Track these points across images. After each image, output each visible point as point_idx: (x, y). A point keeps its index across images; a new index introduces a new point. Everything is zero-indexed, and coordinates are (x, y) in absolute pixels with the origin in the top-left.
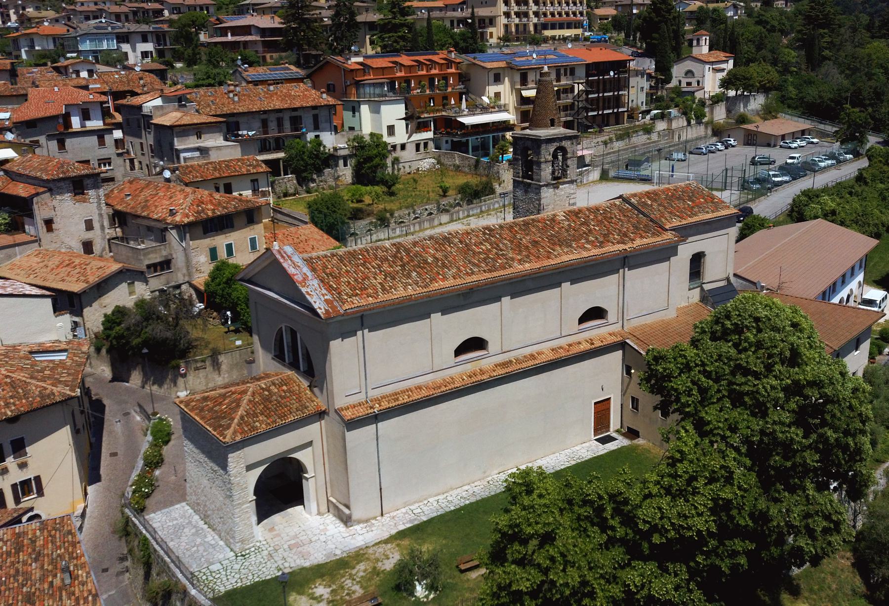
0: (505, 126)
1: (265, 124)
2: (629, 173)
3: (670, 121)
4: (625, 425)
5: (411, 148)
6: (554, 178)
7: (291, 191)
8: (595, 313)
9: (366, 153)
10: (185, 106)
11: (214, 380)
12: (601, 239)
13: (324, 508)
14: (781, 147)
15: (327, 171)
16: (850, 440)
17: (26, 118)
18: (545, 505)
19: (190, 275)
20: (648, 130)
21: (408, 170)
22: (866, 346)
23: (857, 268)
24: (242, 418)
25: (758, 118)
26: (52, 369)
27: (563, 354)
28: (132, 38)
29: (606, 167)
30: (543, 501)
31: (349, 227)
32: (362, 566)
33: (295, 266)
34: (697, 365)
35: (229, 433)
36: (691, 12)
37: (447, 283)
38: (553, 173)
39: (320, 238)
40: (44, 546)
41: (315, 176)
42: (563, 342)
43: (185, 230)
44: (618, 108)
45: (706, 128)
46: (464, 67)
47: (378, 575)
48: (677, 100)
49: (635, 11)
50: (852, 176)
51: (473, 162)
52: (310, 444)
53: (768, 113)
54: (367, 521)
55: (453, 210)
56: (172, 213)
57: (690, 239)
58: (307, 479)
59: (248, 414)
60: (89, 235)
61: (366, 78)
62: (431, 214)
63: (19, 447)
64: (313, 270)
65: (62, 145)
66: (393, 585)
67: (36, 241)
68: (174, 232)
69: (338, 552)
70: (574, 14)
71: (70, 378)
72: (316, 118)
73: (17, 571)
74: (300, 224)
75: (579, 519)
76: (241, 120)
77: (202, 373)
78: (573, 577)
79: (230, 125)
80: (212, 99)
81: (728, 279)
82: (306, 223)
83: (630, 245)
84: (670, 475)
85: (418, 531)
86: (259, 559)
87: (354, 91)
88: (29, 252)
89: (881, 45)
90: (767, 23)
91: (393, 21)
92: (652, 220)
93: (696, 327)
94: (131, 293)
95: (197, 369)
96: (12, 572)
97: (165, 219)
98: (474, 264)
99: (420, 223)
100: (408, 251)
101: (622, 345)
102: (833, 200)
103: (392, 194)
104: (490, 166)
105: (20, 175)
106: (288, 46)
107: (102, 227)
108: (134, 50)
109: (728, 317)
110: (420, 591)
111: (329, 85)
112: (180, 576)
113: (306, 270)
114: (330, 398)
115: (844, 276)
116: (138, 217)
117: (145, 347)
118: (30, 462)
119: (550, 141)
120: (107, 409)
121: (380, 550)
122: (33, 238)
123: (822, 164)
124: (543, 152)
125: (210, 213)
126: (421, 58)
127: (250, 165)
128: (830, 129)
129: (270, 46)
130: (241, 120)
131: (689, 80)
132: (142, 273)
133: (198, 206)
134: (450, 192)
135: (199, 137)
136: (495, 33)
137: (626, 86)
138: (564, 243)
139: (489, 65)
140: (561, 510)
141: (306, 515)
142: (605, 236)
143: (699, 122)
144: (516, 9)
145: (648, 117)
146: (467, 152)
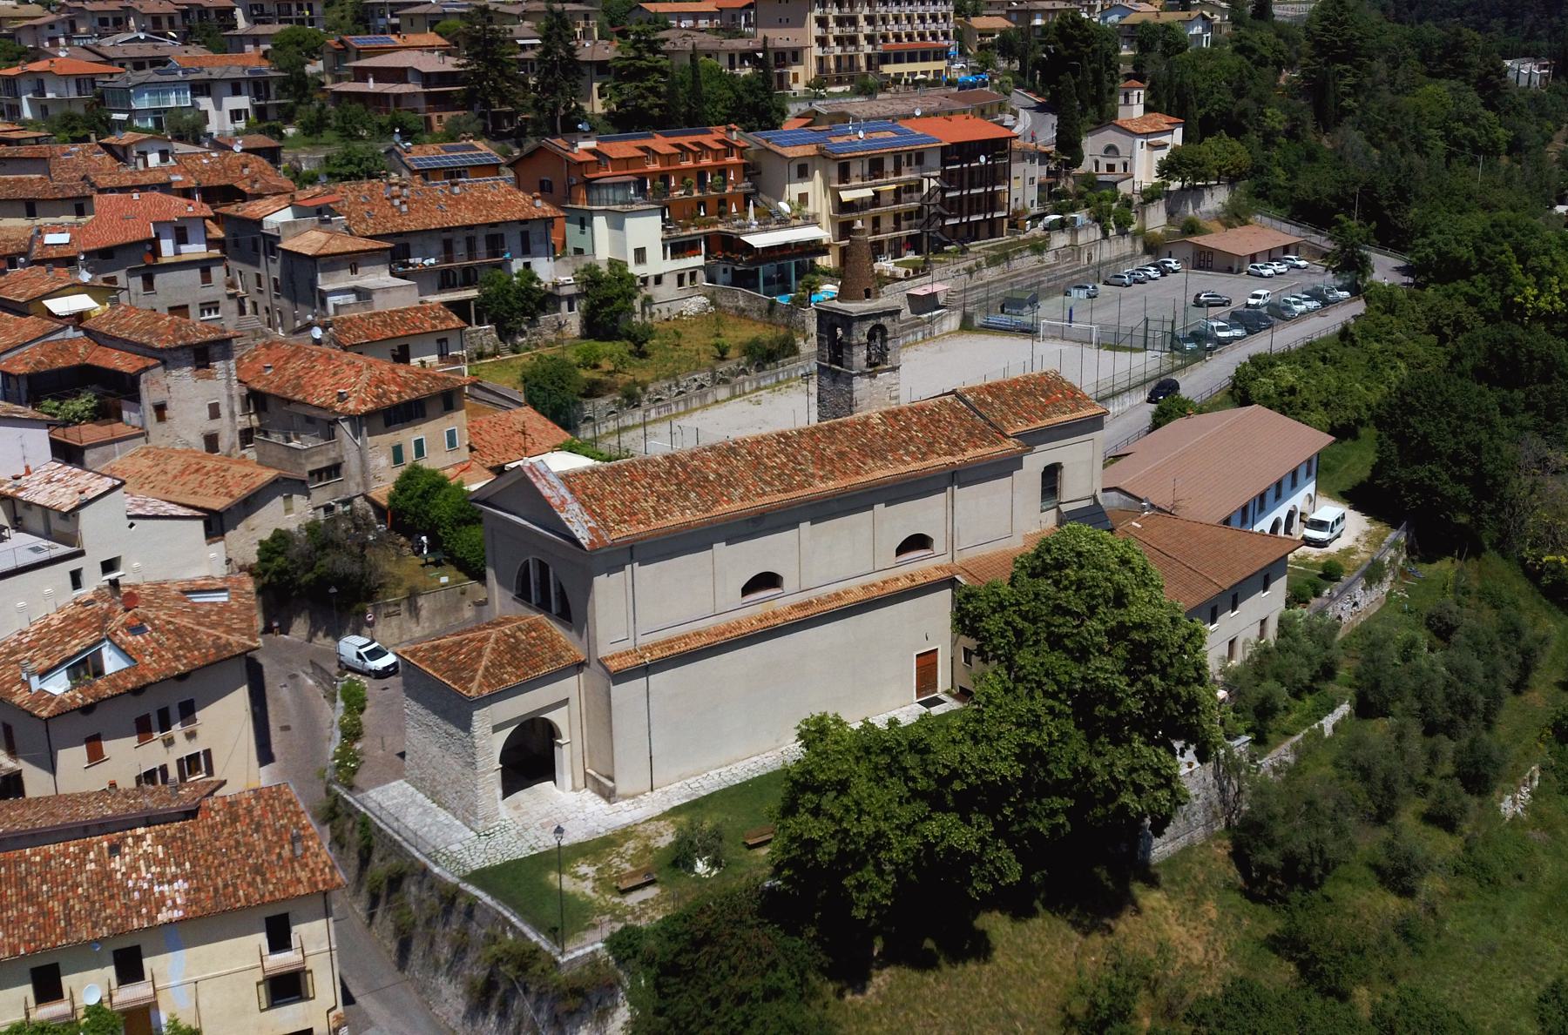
0: (817, 248)
1: (448, 247)
2: (1003, 319)
3: (1075, 232)
4: (957, 684)
5: (670, 282)
6: (871, 365)
7: (489, 350)
8: (918, 542)
9: (603, 292)
10: (329, 221)
11: (410, 630)
12: (924, 450)
13: (580, 782)
14: (1249, 273)
15: (543, 318)
16: (1182, 690)
17: (100, 246)
18: (840, 753)
19: (366, 484)
20: (1038, 248)
21: (665, 315)
22: (1279, 587)
23: (1302, 473)
24: (487, 669)
25: (1217, 224)
26: (218, 613)
27: (875, 593)
28: (215, 89)
29: (969, 309)
30: (836, 747)
31: (583, 409)
32: (631, 844)
33: (551, 487)
34: (1011, 605)
35: (474, 686)
36: (1133, 26)
37: (733, 506)
38: (869, 358)
39: (541, 427)
40: (263, 816)
41: (525, 327)
42: (877, 578)
43: (361, 422)
44: (993, 210)
45: (1134, 241)
46: (751, 152)
47: (651, 852)
48: (1090, 195)
49: (1038, 22)
50: (1331, 331)
51: (765, 305)
52: (566, 702)
53: (1234, 217)
54: (633, 797)
55: (734, 380)
56: (342, 398)
57: (1038, 448)
58: (561, 746)
59: (493, 665)
60: (213, 426)
61: (601, 174)
62: (702, 386)
63: (187, 712)
64: (572, 491)
65: (149, 283)
66: (669, 861)
67: (142, 435)
68: (346, 425)
69: (601, 830)
70: (934, 36)
71: (244, 625)
72: (525, 238)
73: (238, 842)
74: (511, 405)
75: (876, 768)
76: (412, 241)
77: (394, 621)
78: (868, 827)
79: (396, 252)
80: (367, 208)
81: (1094, 497)
82: (520, 404)
83: (960, 457)
84: (977, 721)
85: (696, 806)
86: (507, 838)
87: (582, 194)
88: (132, 451)
89: (1440, 90)
90: (1254, 51)
91: (638, 63)
92: (990, 424)
93: (1016, 561)
94: (288, 510)
95: (388, 615)
96: (232, 843)
97: (331, 407)
98: (766, 483)
99: (685, 401)
100: (684, 465)
101: (951, 583)
102: (1294, 372)
103: (643, 355)
104: (792, 310)
105: (114, 338)
106: (467, 102)
107: (232, 414)
108: (219, 107)
109: (1048, 551)
110: (701, 867)
111: (542, 182)
112: (417, 854)
113: (563, 491)
114: (591, 645)
115: (1279, 484)
116: (289, 401)
117: (310, 586)
118: (200, 730)
119: (864, 318)
120: (265, 670)
121: (652, 827)
122: (136, 431)
123: (1299, 308)
124: (855, 332)
125: (395, 398)
126: (685, 141)
127: (435, 318)
128: (1322, 241)
129: (439, 102)
130: (412, 241)
131: (1111, 161)
132: (303, 482)
133: (377, 387)
134: (732, 353)
135: (354, 271)
136: (802, 74)
137: (1006, 176)
138: (878, 455)
139: (790, 152)
140: (858, 759)
141: (556, 791)
142: (930, 445)
143: (1122, 232)
144: (837, 31)
145: (1041, 225)
146: (755, 287)
